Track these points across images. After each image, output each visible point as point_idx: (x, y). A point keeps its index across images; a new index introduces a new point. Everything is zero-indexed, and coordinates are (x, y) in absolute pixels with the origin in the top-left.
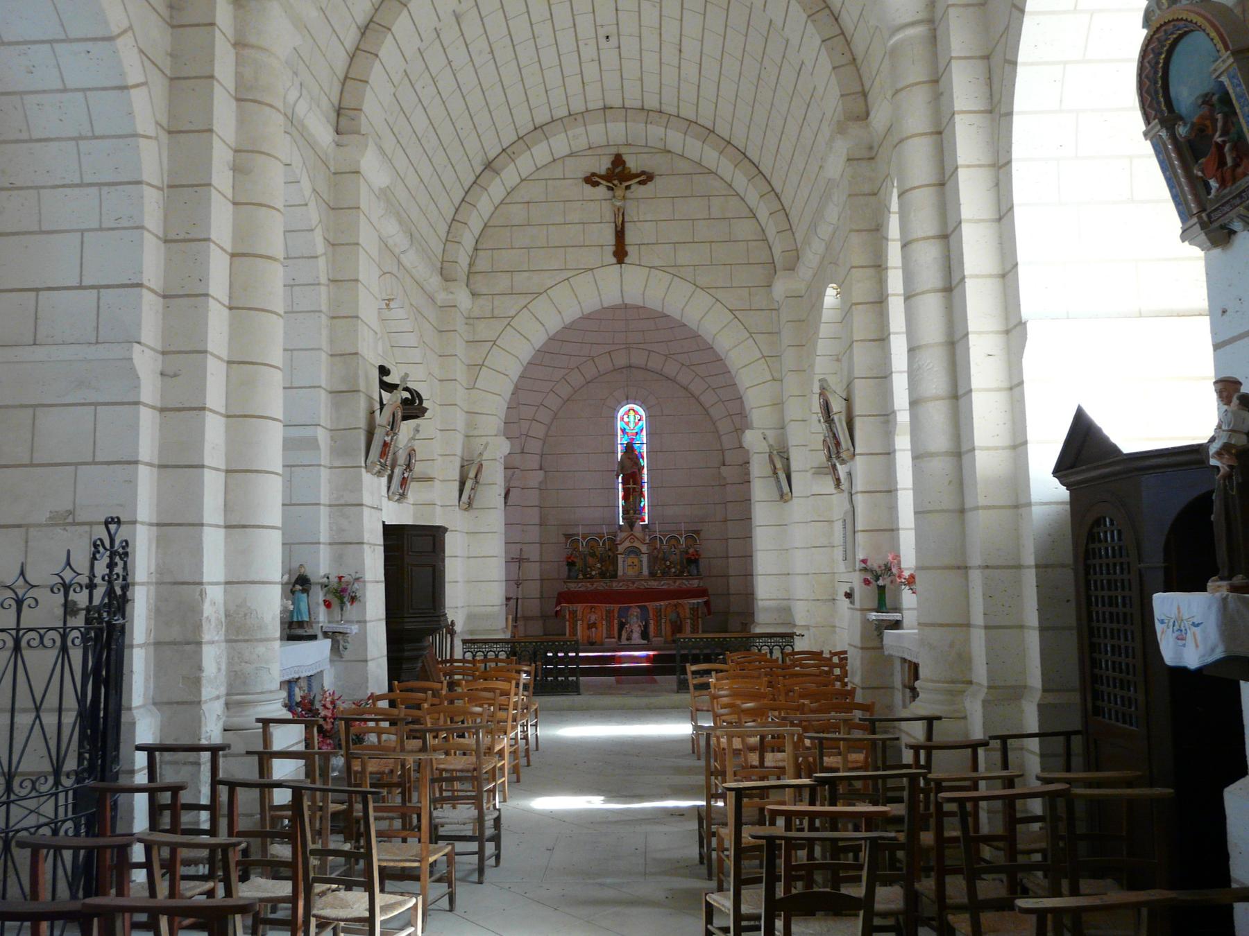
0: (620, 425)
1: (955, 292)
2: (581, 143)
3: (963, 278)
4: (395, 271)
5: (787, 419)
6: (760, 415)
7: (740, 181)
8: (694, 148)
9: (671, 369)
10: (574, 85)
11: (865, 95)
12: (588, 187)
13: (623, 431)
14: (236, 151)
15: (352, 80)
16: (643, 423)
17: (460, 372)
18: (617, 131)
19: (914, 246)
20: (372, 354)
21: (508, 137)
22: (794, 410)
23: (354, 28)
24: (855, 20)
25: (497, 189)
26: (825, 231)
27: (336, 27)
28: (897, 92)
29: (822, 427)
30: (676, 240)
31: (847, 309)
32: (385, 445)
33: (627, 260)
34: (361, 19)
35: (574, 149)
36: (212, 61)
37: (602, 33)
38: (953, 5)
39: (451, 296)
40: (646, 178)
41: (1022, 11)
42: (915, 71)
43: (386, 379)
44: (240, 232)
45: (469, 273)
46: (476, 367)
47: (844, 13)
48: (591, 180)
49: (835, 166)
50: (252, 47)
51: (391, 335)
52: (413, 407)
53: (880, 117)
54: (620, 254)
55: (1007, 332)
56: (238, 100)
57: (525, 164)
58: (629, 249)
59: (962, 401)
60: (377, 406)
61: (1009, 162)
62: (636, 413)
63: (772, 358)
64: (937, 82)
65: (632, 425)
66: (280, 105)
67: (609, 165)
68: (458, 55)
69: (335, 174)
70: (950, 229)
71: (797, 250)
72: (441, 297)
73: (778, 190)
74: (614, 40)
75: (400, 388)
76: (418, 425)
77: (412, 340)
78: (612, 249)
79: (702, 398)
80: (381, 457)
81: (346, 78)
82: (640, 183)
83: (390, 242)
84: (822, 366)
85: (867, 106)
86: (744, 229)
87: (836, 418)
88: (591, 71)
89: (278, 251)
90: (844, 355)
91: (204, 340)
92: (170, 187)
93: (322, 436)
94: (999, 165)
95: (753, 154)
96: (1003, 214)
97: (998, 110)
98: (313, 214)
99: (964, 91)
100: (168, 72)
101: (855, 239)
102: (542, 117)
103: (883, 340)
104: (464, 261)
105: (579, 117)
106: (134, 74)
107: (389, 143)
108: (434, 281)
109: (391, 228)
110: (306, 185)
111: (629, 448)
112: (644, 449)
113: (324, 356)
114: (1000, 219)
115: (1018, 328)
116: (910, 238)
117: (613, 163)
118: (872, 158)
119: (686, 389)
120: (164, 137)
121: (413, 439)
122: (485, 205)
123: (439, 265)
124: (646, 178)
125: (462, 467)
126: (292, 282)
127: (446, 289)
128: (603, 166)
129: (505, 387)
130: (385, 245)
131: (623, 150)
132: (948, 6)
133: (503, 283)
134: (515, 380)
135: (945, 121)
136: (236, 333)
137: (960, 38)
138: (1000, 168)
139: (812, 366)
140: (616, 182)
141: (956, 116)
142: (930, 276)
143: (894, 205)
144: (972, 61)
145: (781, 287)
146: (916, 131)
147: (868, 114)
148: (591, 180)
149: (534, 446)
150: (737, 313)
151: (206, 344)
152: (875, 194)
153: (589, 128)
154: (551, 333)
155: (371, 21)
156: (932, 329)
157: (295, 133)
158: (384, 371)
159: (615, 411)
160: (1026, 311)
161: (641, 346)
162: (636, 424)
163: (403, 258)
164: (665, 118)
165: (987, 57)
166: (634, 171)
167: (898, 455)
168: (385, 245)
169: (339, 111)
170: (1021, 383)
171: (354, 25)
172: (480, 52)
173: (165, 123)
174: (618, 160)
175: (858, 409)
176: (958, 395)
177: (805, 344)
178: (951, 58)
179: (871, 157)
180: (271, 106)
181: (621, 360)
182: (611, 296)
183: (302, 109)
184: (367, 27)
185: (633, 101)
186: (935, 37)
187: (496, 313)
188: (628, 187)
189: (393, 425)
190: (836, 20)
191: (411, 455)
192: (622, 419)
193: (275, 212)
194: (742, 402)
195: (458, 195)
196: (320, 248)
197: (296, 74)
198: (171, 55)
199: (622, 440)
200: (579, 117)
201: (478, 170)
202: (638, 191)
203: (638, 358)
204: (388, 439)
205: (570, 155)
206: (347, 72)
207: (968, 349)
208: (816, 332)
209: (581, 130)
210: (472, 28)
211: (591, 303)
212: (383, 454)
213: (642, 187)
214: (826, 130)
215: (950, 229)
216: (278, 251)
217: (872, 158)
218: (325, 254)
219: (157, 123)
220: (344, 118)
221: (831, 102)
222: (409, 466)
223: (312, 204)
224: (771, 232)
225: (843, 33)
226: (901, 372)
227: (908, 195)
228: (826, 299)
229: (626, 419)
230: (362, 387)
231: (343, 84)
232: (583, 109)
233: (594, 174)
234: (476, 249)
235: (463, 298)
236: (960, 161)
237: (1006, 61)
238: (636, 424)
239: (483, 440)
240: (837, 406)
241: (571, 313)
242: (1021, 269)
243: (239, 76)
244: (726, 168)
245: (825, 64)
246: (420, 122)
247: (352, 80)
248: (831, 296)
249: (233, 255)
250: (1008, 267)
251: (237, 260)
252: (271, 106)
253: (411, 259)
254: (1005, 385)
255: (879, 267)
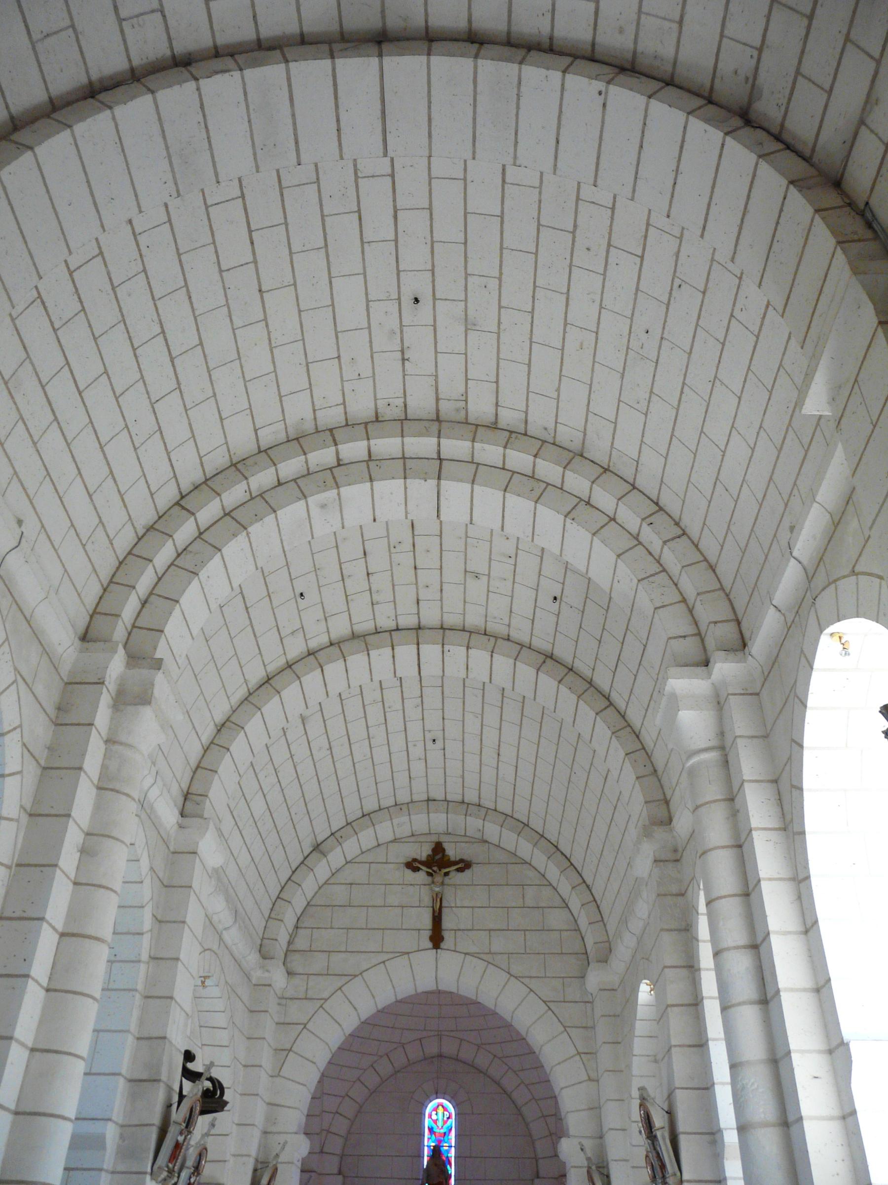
0: (427, 1123)
1: (771, 1004)
2: (405, 831)
3: (778, 992)
4: (215, 948)
5: (605, 1129)
6: (576, 1122)
7: (553, 873)
8: (509, 839)
9: (482, 1060)
10: (402, 779)
11: (667, 802)
12: (408, 872)
13: (431, 1130)
14: (88, 834)
15: (202, 769)
16: (452, 1122)
17: (266, 1059)
18: (439, 821)
19: (726, 955)
20: (179, 1039)
21: (338, 822)
22: (612, 1117)
23: (212, 725)
24: (654, 739)
25: (322, 871)
26: (636, 925)
27: (196, 725)
28: (697, 807)
29: (641, 1140)
30: (491, 926)
31: (663, 1010)
32: (178, 1146)
33: (442, 945)
34: (219, 718)
35: (398, 836)
36: (83, 755)
37: (429, 736)
38: (740, 736)
39: (266, 975)
40: (464, 865)
41: (801, 746)
42: (712, 790)
43: (190, 1066)
44: (75, 912)
45: (287, 951)
46: (283, 1052)
47: (643, 731)
48: (412, 865)
49: (643, 866)
50: (121, 744)
51: (204, 1021)
52: (213, 1100)
53: (683, 822)
54: (437, 939)
55: (830, 1052)
56: (99, 788)
57: (351, 847)
58: (446, 934)
59: (794, 1129)
60: (176, 1098)
61: (808, 877)
62: (445, 1109)
63: (588, 1054)
64: (732, 799)
65: (440, 1124)
66: (136, 795)
67: (430, 852)
68: (300, 750)
69: (174, 853)
70: (759, 940)
71: (609, 941)
72: (257, 975)
73: (589, 882)
74: (439, 744)
75: (203, 1078)
76: (215, 1119)
77: (221, 1020)
78: (428, 933)
79: (515, 1095)
80: (170, 1161)
81: (198, 767)
82: (458, 870)
83: (215, 919)
84: (641, 1074)
85: (669, 812)
86: (557, 919)
87: (659, 1134)
88: (418, 768)
89: (107, 932)
90: (662, 1058)
91: (13, 1025)
92: (18, 865)
93: (111, 1133)
94: (799, 880)
95: (565, 847)
96: (809, 928)
97: (791, 828)
98: (146, 892)
99: (758, 810)
100: (42, 763)
101: (667, 939)
102: (370, 805)
103: (707, 1089)
104: (283, 938)
105: (404, 808)
106: (13, 764)
107: (227, 825)
108: (252, 958)
109: (218, 906)
110: (145, 863)
111: (436, 1152)
112: (452, 1154)
113: (130, 1039)
114: (806, 932)
115: (841, 1049)
116: (714, 896)
117: (434, 850)
118: (677, 861)
119: (498, 1083)
120: (24, 819)
121: (207, 1134)
122: (309, 885)
123: (259, 942)
124: (464, 865)
125: (255, 1170)
126: (113, 958)
127: (262, 967)
128: (424, 852)
129: (312, 1076)
130: (209, 920)
131: (443, 839)
132: (736, 737)
133: (319, 963)
134: (322, 1069)
135: (743, 837)
136: (49, 1017)
137: (749, 764)
138: (800, 882)
139: (629, 1066)
140: (435, 868)
141: (753, 832)
142: (744, 987)
143: (702, 908)
144: (763, 784)
145: (595, 978)
146: (718, 844)
147: (670, 820)
148: (412, 865)
149: (335, 1145)
150: (551, 1005)
151: (14, 1029)
152: (683, 895)
153: (413, 817)
154: (363, 1018)
155: (228, 720)
156: (753, 1048)
157: (144, 816)
158: (189, 1056)
159: (424, 1106)
160: (847, 1032)
161: (452, 1034)
162: (445, 1122)
163: (226, 936)
164: (483, 811)
165: (775, 781)
166: (453, 859)
167: (718, 1089)
168: (209, 920)
169: (187, 796)
170: (854, 1113)
171: (212, 723)
172: (320, 749)
173: (28, 806)
174: (438, 848)
175: (681, 1127)
176: (788, 1122)
177: (621, 1040)
178: (743, 781)
179: (677, 861)
180: (128, 795)
181: (432, 1049)
182: (426, 983)
183: (154, 794)
184: (223, 725)
185: (454, 794)
186: (727, 762)
187: (310, 994)
188: (446, 874)
189: (189, 1122)
190: (638, 737)
191: (202, 1154)
192: (430, 1116)
193: (113, 894)
194: (557, 1103)
195: (285, 874)
196: (147, 922)
197: (154, 763)
198: (48, 748)
199: (429, 1142)
200: (404, 808)
201: (307, 851)
202: (456, 878)
203: (449, 1047)
204: (181, 1139)
205: (395, 841)
206: (200, 762)
207: (792, 1070)
208: (632, 1027)
209: (405, 819)
210: (315, 728)
211: (405, 988)
212: (173, 1157)
213: (460, 875)
214: (633, 833)
215: (759, 940)
216: (107, 932)
217: (677, 861)
218: (151, 930)
219: (21, 807)
220: (190, 803)
221: (636, 805)
222: (197, 1169)
223: (147, 882)
224: (583, 923)
225: (644, 748)
226: (723, 1084)
227: (703, 810)
228: (640, 994)
229: (434, 1117)
230: (164, 1077)
231: (194, 773)
232: (409, 800)
233: (415, 860)
234: (297, 927)
235: (278, 978)
236: (762, 874)
237: (793, 786)
238: (445, 1122)
239: (281, 1139)
240: (659, 1121)
241: (385, 997)
242: (834, 984)
243: (104, 767)
244: (539, 859)
245: (629, 774)
246: (258, 806)
247: (202, 769)
248: (645, 992)
249: (62, 935)
250: (822, 983)
251: (66, 939)
252: (128, 795)
253: (233, 936)
254: (836, 1112)
255: (692, 968)
